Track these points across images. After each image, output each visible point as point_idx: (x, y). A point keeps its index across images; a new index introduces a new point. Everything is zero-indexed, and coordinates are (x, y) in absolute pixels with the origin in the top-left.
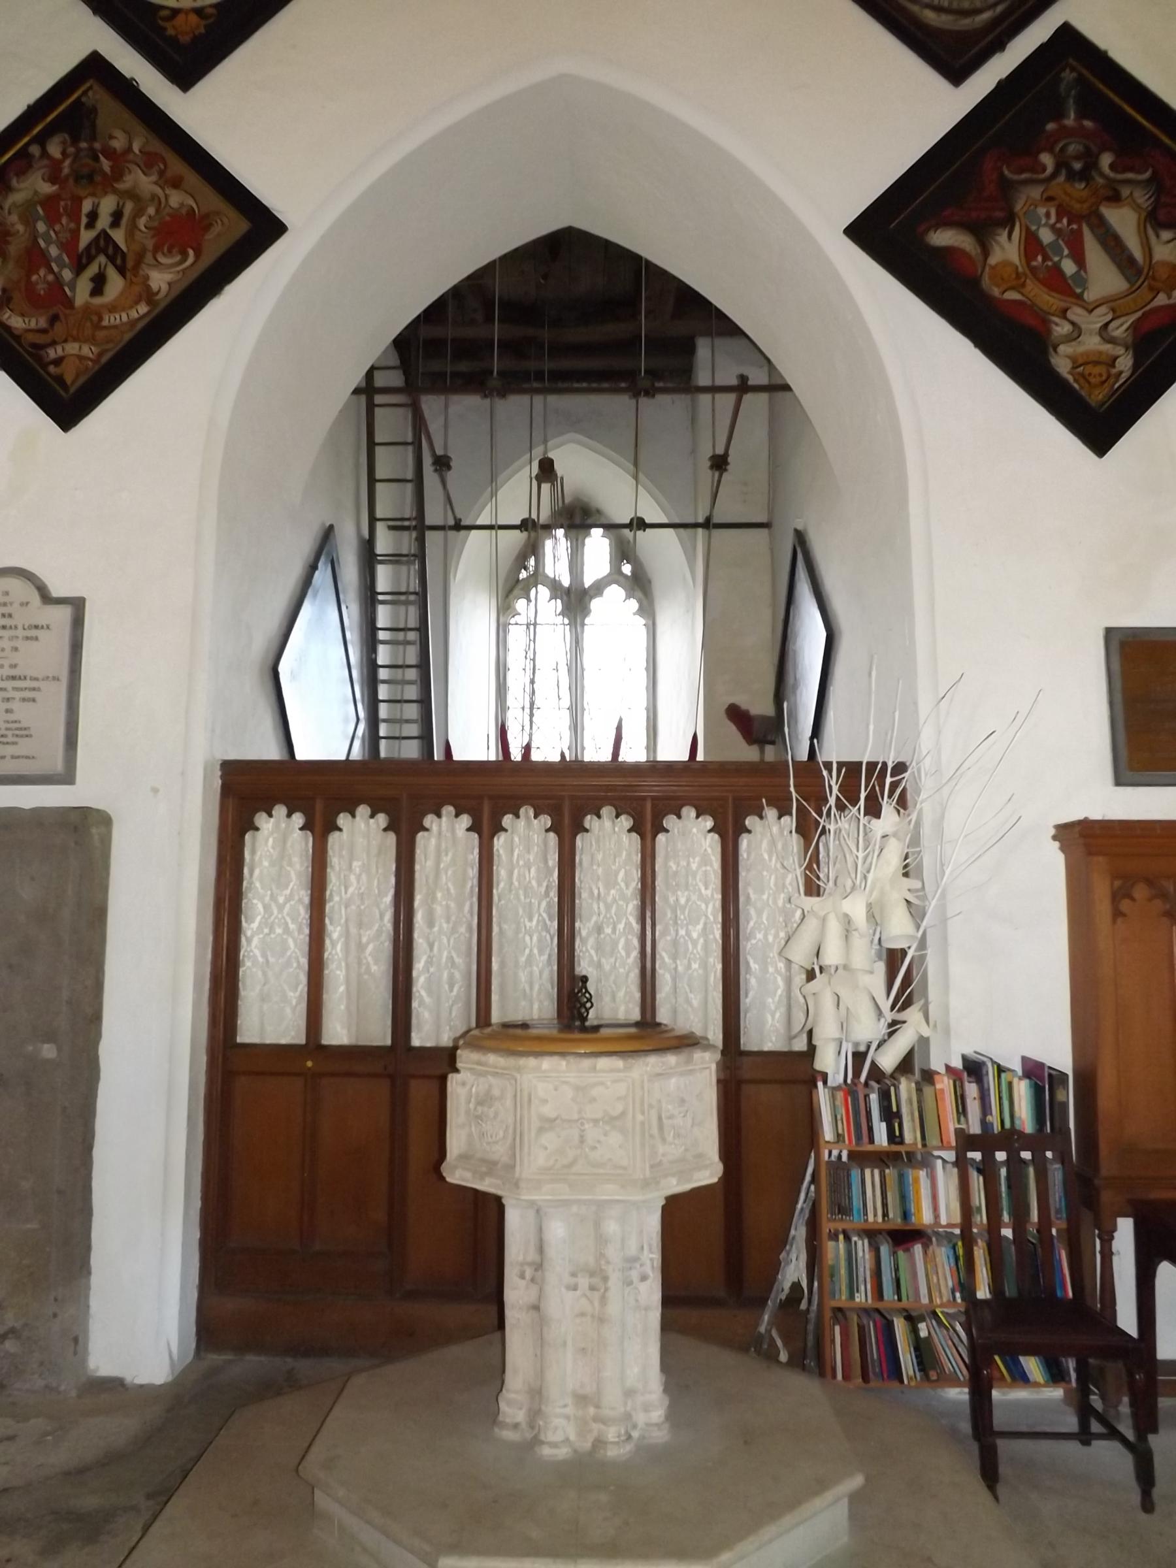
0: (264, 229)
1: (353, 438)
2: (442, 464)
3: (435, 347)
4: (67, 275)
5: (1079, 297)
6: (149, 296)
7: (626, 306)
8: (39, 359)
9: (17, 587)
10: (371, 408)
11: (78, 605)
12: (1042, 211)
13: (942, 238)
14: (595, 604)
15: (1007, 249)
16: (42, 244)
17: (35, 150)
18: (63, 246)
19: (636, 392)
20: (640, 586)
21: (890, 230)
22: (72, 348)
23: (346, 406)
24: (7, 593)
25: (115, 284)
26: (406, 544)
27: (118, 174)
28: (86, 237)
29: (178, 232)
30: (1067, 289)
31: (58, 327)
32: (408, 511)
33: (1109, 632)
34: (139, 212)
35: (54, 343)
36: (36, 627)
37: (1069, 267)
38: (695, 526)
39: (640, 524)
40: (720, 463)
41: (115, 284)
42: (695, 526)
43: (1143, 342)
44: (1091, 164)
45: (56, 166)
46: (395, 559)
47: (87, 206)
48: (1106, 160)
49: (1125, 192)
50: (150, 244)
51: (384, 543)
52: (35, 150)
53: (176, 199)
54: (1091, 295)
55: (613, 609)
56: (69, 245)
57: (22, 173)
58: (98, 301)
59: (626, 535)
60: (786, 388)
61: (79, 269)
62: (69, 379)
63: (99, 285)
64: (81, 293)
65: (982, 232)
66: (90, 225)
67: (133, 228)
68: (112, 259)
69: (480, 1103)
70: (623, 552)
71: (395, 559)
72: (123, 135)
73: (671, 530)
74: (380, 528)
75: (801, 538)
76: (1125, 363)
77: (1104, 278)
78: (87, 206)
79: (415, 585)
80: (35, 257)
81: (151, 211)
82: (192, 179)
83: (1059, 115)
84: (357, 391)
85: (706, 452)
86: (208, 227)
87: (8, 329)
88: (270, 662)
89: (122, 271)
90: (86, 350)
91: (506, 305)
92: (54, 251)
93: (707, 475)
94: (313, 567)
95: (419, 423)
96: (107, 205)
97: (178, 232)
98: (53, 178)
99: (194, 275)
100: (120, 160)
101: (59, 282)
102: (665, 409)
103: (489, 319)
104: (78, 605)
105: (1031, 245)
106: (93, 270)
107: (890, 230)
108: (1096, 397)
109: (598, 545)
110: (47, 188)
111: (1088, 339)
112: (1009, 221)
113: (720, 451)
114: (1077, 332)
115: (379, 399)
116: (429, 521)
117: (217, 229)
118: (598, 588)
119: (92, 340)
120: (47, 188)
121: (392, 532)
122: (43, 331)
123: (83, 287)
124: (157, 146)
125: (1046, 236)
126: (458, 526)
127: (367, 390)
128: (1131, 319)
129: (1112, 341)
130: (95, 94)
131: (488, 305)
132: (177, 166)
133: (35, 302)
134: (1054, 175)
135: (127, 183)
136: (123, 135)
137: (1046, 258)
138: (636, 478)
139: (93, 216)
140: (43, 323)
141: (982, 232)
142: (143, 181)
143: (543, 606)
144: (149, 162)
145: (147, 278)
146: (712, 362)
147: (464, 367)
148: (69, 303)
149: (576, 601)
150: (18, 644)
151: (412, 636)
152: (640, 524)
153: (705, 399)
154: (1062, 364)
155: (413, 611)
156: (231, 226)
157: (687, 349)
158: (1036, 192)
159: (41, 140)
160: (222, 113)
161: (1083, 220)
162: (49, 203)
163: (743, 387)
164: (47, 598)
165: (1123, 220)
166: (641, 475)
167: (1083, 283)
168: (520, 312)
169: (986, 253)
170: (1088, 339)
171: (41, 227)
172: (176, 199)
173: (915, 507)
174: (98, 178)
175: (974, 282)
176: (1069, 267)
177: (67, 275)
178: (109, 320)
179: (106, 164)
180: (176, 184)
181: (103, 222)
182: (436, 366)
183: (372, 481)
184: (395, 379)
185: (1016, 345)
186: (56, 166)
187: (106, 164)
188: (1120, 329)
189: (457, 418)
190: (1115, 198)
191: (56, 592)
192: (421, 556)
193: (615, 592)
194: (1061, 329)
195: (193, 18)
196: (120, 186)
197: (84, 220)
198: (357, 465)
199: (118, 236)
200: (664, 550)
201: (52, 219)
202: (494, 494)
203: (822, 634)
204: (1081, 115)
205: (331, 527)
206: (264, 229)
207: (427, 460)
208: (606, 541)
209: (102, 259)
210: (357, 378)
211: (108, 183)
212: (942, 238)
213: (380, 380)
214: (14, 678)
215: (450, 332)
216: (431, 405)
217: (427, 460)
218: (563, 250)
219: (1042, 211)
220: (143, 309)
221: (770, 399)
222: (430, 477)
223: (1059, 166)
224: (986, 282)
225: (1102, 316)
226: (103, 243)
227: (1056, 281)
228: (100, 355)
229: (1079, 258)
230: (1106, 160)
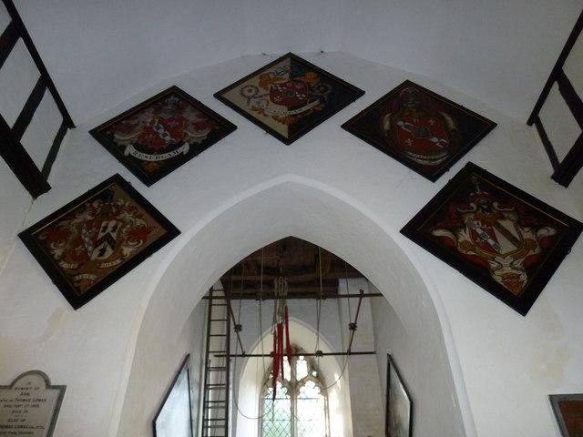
0: (171, 232)
1: (203, 319)
2: (238, 328)
3: (237, 284)
4: (90, 248)
5: (498, 254)
6: (122, 257)
7: (314, 267)
8: (71, 280)
9: (36, 380)
10: (211, 305)
11: (62, 389)
12: (476, 223)
13: (439, 233)
14: (302, 389)
15: (465, 236)
16: (83, 237)
17: (88, 205)
18: (92, 239)
19: (318, 298)
20: (321, 381)
21: (417, 230)
22: (86, 276)
23: (200, 303)
24: (30, 383)
25: (109, 252)
26: (222, 362)
27: (118, 213)
28: (101, 235)
29: (137, 234)
30: (494, 251)
31: (82, 267)
32: (224, 348)
33: (552, 398)
34: (123, 227)
35: (79, 274)
36: (39, 400)
37: (491, 242)
38: (344, 354)
39: (320, 354)
40: (353, 327)
41: (109, 252)
42: (344, 354)
43: (528, 268)
44: (490, 206)
45: (95, 210)
46: (218, 369)
47: (104, 224)
48: (495, 205)
49: (506, 215)
50: (126, 237)
51: (214, 362)
52: (88, 205)
53: (139, 222)
54: (503, 252)
55: (310, 389)
56: (93, 238)
57: (81, 212)
58: (100, 258)
59: (313, 358)
60: (380, 295)
61: (96, 246)
62: (81, 289)
63: (102, 252)
64: (94, 256)
65: (454, 231)
66: (104, 231)
67: (120, 231)
68: (109, 243)
69: (311, 89)
70: (312, 367)
71: (218, 369)
72: (122, 200)
73: (333, 356)
74: (211, 356)
75: (390, 358)
76: (524, 277)
77: (506, 246)
78: (104, 224)
79: (224, 382)
80: (79, 241)
81: (129, 226)
82: (147, 215)
83: (474, 191)
84: (204, 298)
85: (346, 322)
86: (149, 233)
87: (61, 268)
88: (153, 418)
89: (113, 247)
90: (92, 277)
91: (266, 268)
92: (87, 240)
93: (347, 331)
94: (179, 372)
95: (230, 311)
96: (112, 224)
97: (137, 234)
98: (93, 215)
99: (142, 249)
100: (120, 209)
101: (86, 251)
102: (329, 303)
103: (259, 274)
104: (62, 389)
105: (474, 235)
106: (101, 247)
107: (417, 230)
108: (516, 292)
109: (302, 366)
110: (90, 218)
111: (506, 266)
112: (464, 226)
113: (353, 322)
114: (501, 267)
115: (214, 301)
116: (231, 353)
117: (153, 233)
118: (303, 382)
119: (95, 273)
120: (90, 218)
121: (217, 358)
122: (76, 269)
123: (97, 252)
124: (135, 204)
125: (480, 231)
126: (244, 355)
127: (209, 297)
128: (521, 260)
129: (516, 269)
130: (115, 187)
131: (259, 267)
132: (141, 211)
133: (75, 259)
134: (478, 209)
135: (122, 216)
136: (122, 200)
137: (481, 239)
138: (318, 335)
139: (106, 228)
140: (76, 266)
141: (454, 231)
142: (128, 216)
143: (281, 391)
144: (131, 209)
145: (122, 250)
146: (345, 286)
147: (249, 291)
148: (89, 259)
149: (293, 388)
150: (29, 409)
151: (223, 404)
152: (320, 354)
153: (344, 300)
154: (498, 278)
155: (223, 392)
156: (159, 231)
157: (335, 284)
158: (472, 216)
159: (90, 202)
160: (164, 196)
161: (492, 224)
162: (89, 224)
163: (362, 295)
164: (48, 385)
165: (508, 225)
166: (320, 334)
167: (499, 248)
168: (272, 271)
169: (457, 238)
170: (506, 266)
171: (84, 231)
172: (139, 222)
173: (447, 340)
174: (110, 215)
175: (455, 248)
176: (491, 242)
177: (90, 248)
178: (104, 265)
179: (114, 210)
180: (140, 217)
181: (109, 230)
182: (237, 291)
183: (209, 335)
184: (221, 294)
185: (477, 272)
186: (95, 210)
187: (114, 210)
188: (518, 264)
189: (246, 310)
190: (503, 218)
191: (53, 383)
192: (227, 369)
193: (311, 384)
194: (494, 265)
195: (155, 164)
196: (118, 218)
197: (102, 229)
198: (203, 329)
199: (114, 235)
200: (329, 365)
201: (89, 228)
202: (261, 339)
203: (408, 402)
204: (482, 190)
205: (189, 355)
206: (171, 232)
207: (232, 327)
208: (305, 362)
209: (106, 243)
210: (205, 292)
211: (114, 217)
212: (439, 233)
213: (215, 294)
214: (22, 427)
215: (242, 278)
216: (234, 303)
217: (232, 327)
218: (288, 245)
219: (476, 223)
220: (118, 261)
221: (371, 301)
222: (233, 335)
223: (478, 207)
224: (459, 248)
225: (509, 260)
226: (108, 238)
227: (487, 247)
228: (97, 279)
229: (494, 238)
230: (495, 205)
